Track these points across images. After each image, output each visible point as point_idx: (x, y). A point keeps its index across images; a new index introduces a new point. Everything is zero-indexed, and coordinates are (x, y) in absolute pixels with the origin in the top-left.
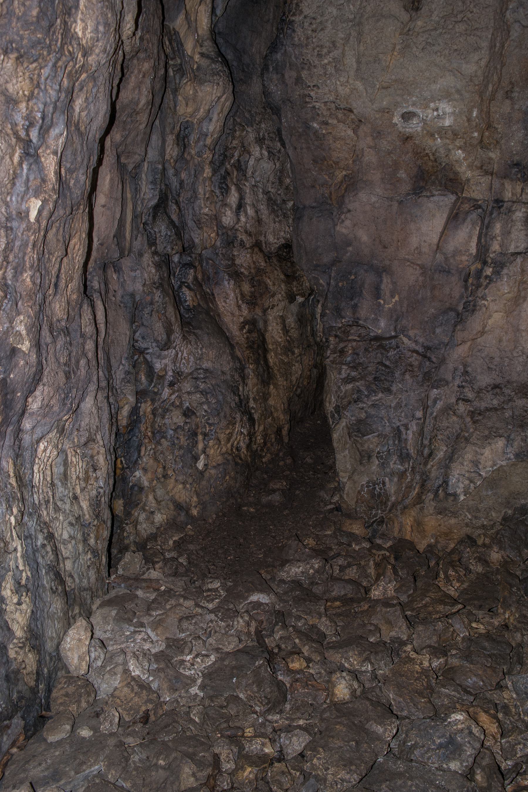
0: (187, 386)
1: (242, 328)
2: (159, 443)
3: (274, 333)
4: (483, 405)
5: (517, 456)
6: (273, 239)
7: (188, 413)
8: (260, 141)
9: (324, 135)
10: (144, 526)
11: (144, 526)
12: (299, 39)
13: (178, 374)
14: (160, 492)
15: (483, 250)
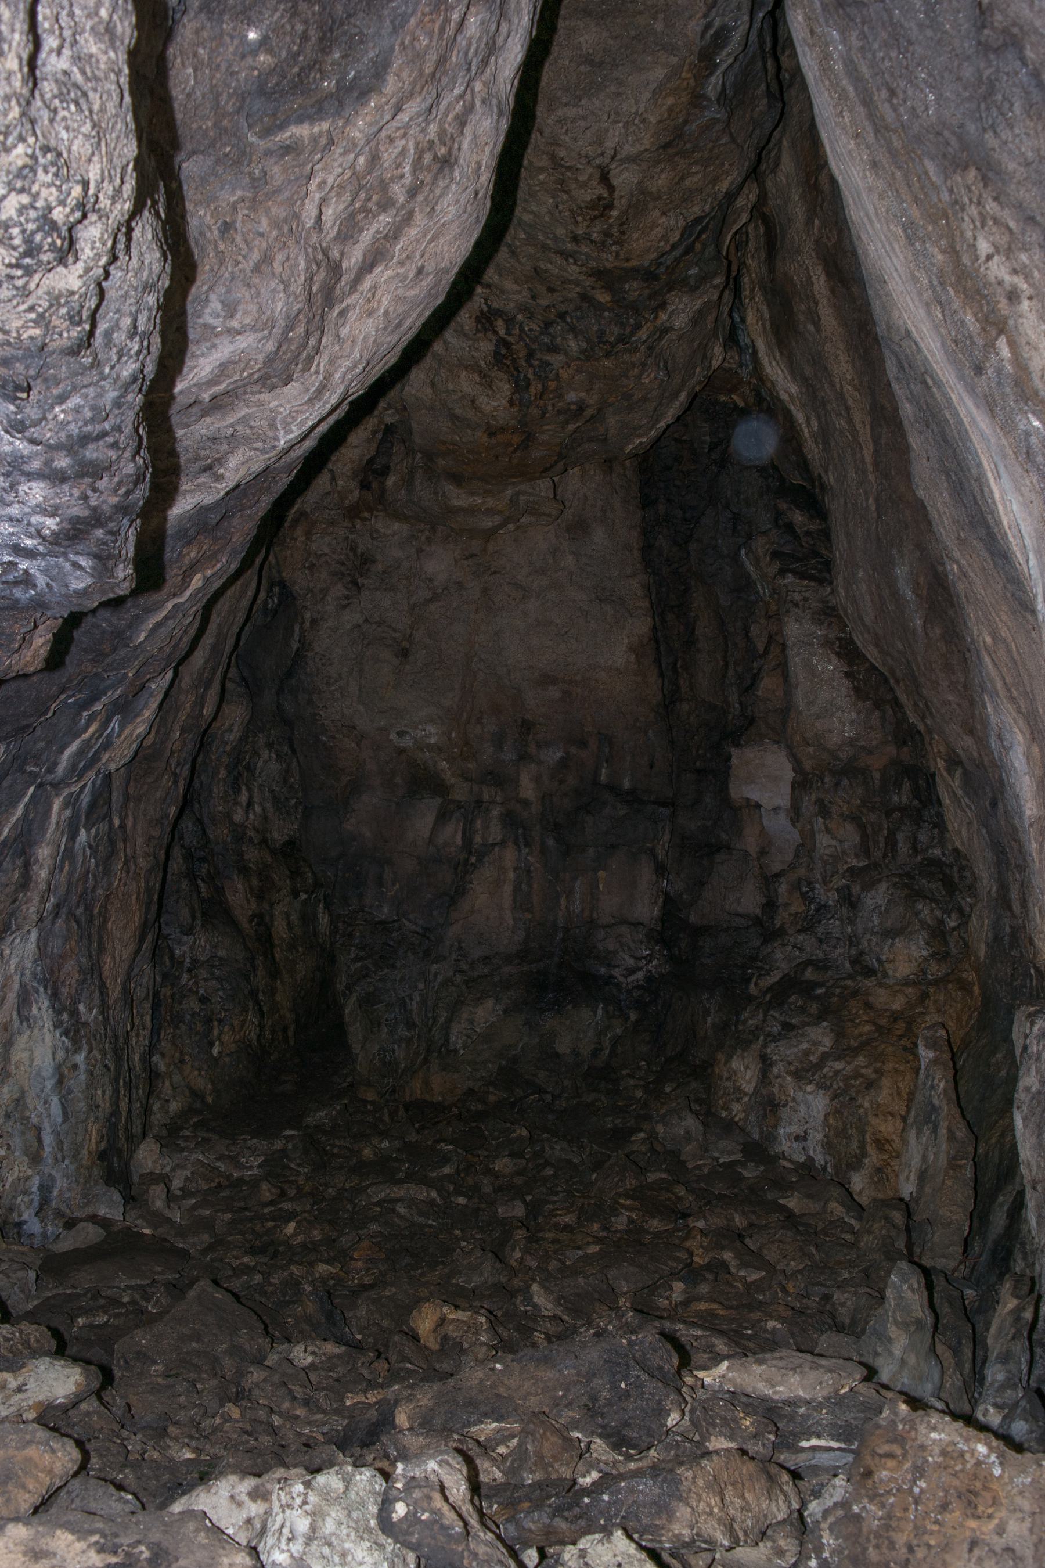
0: (204, 973)
1: (250, 922)
2: (177, 1027)
3: (280, 928)
4: (476, 974)
5: (505, 1012)
6: (279, 834)
7: (204, 1000)
8: (269, 746)
10: (158, 1116)
11: (158, 1116)
13: (195, 961)
14: (176, 1078)
15: (468, 841)
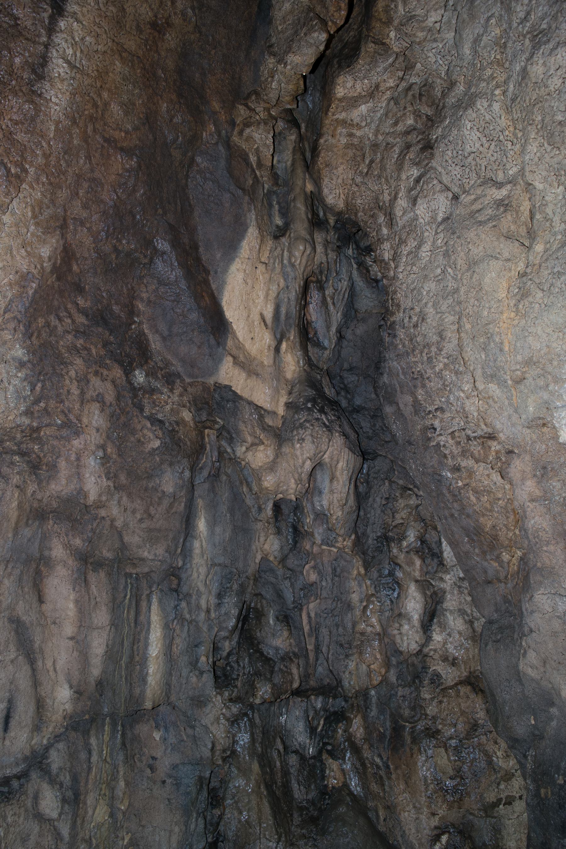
9: (460, 488)
12: (404, 346)
